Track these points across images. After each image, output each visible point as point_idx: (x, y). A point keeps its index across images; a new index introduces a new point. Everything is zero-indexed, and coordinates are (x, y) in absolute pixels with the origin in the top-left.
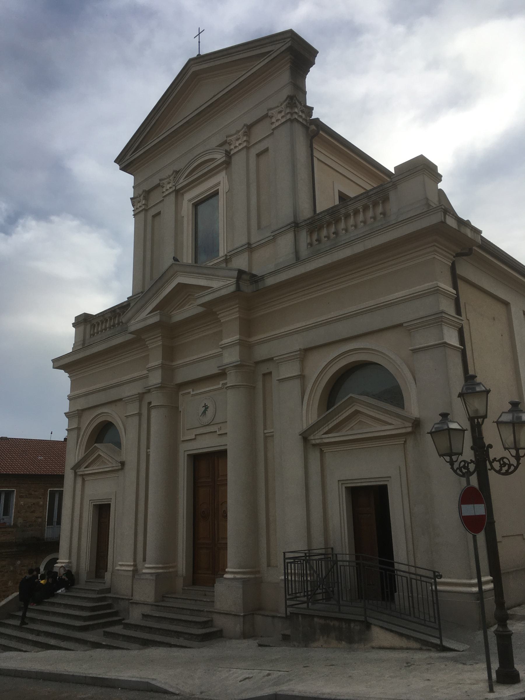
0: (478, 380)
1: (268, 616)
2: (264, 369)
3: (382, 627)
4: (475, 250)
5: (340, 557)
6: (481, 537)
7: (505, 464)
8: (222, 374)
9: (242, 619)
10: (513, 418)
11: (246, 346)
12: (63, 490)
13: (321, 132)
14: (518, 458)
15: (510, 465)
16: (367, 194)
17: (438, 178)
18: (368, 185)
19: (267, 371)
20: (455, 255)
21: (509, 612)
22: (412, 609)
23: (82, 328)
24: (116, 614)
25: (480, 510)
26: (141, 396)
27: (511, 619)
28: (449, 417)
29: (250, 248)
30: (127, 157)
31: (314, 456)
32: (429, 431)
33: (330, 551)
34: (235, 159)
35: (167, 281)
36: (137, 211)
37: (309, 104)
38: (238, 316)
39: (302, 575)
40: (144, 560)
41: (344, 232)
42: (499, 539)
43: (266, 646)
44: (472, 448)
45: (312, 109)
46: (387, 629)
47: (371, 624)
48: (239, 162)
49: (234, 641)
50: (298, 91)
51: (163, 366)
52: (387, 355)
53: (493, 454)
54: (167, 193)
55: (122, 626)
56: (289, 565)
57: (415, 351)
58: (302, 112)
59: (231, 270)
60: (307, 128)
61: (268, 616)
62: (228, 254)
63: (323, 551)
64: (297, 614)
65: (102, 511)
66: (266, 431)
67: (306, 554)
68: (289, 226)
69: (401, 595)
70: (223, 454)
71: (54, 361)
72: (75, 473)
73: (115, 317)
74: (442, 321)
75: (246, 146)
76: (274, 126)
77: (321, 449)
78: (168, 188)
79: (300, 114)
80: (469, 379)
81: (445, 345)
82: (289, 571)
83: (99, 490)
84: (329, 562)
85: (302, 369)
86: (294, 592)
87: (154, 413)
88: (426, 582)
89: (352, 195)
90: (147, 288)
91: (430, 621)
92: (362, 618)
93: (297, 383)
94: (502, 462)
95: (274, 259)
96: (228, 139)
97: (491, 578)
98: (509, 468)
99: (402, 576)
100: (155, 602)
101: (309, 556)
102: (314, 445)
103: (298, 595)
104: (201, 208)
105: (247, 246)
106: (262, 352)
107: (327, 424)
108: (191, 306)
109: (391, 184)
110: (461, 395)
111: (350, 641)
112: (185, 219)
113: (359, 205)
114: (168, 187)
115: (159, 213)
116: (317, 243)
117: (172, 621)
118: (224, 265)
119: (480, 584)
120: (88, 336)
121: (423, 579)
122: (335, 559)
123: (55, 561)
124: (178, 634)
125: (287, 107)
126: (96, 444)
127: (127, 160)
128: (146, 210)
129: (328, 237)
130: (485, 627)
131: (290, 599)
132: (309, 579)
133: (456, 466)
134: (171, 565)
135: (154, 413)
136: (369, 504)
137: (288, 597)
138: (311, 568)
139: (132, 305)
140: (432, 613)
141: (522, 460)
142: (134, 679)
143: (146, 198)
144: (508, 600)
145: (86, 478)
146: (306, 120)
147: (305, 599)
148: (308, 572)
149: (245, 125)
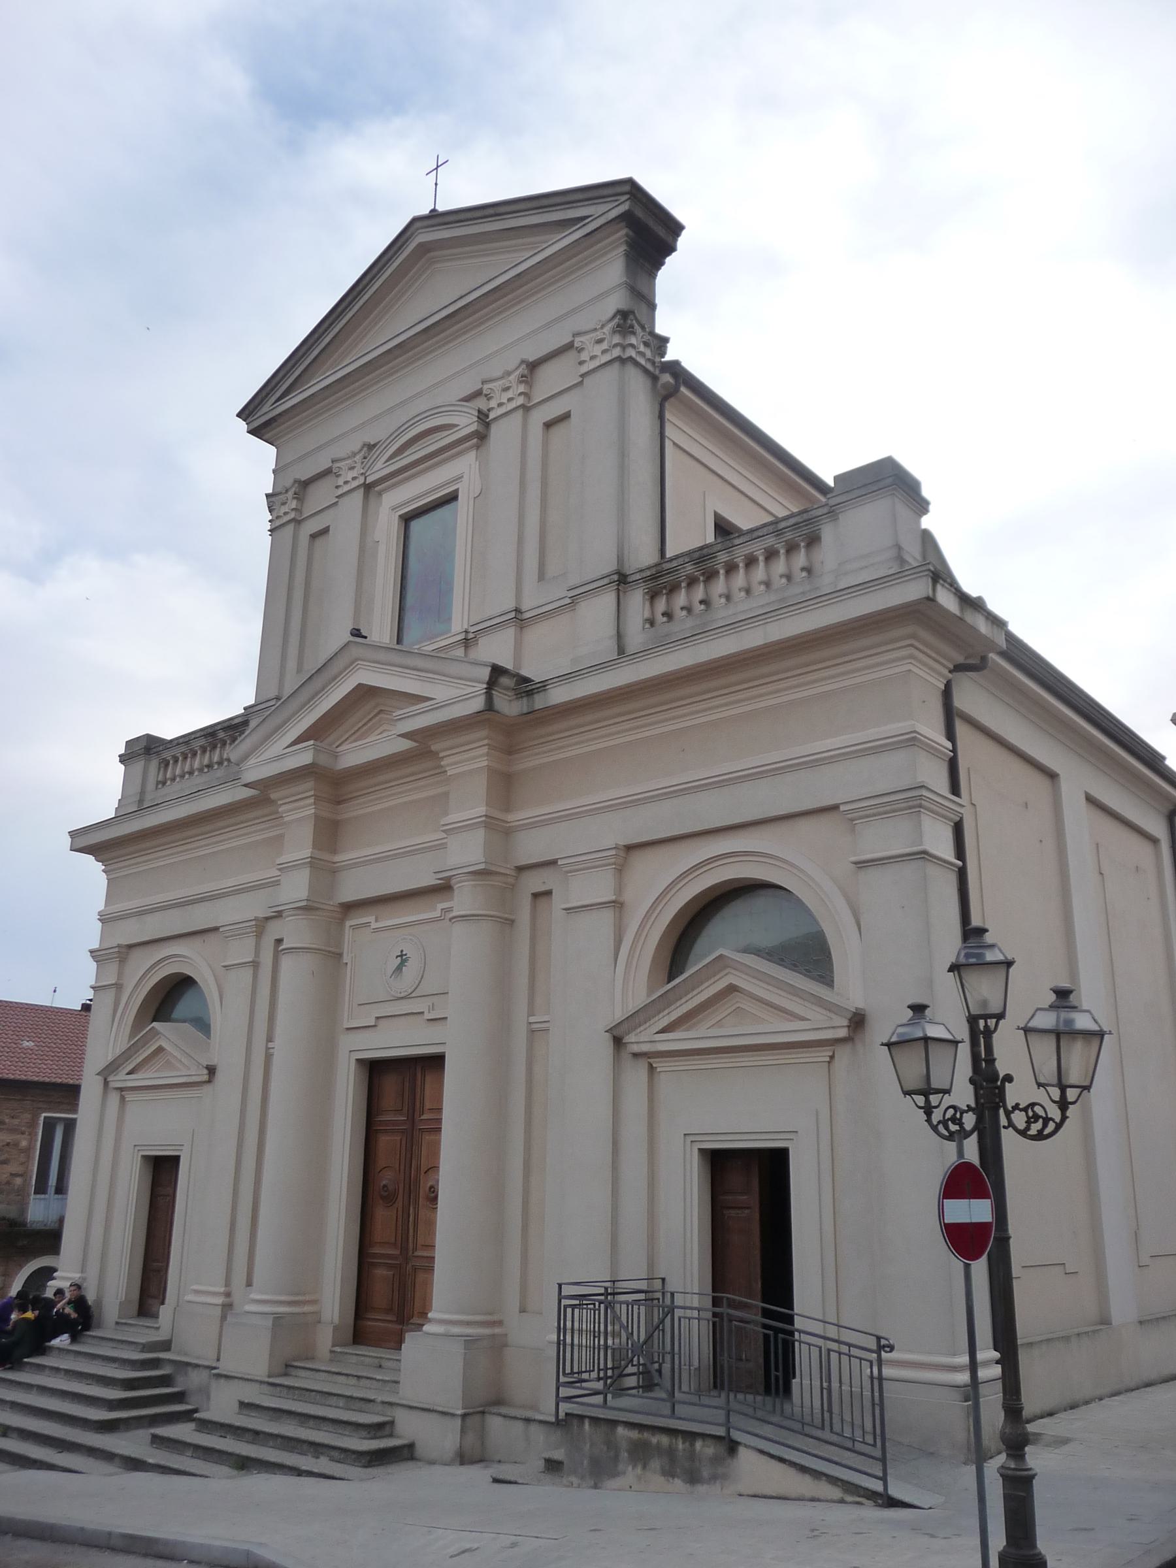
0: (989, 938)
1: (515, 1418)
2: (535, 882)
3: (762, 1452)
4: (993, 660)
5: (679, 1300)
6: (980, 1267)
7: (1036, 1117)
8: (444, 888)
9: (459, 1422)
10: (1058, 1021)
11: (498, 829)
12: (75, 1120)
13: (683, 389)
14: (1063, 1105)
15: (1046, 1120)
16: (775, 527)
17: (922, 506)
18: (781, 506)
19: (543, 888)
20: (951, 667)
21: (1031, 1428)
22: (827, 1415)
23: (139, 766)
24: (180, 1397)
25: (978, 1211)
26: (261, 925)
27: (1034, 1443)
28: (927, 1012)
29: (519, 619)
30: (265, 409)
31: (636, 1076)
32: (885, 1041)
33: (657, 1284)
34: (497, 432)
35: (335, 678)
36: (278, 523)
37: (660, 329)
38: (486, 763)
39: (595, 1335)
40: (249, 1284)
41: (723, 600)
42: (1016, 1271)
43: (510, 1482)
44: (971, 1081)
45: (665, 340)
46: (772, 1456)
47: (738, 1443)
48: (504, 434)
49: (438, 1470)
50: (635, 316)
51: (314, 863)
52: (792, 865)
53: (1013, 1095)
54: (346, 488)
55: (192, 1426)
56: (569, 1310)
57: (862, 865)
58: (646, 344)
59: (475, 663)
60: (655, 379)
61: (515, 1418)
62: (472, 629)
63: (643, 1285)
64: (581, 1418)
65: (162, 1170)
66: (532, 1019)
67: (606, 1289)
68: (606, 581)
69: (806, 1384)
70: (436, 1062)
71: (73, 834)
72: (106, 1083)
73: (214, 747)
74: (920, 806)
75: (523, 406)
76: (584, 369)
77: (650, 1065)
78: (281, 514)
79: (642, 348)
80: (972, 933)
81: (924, 855)
82: (569, 1324)
83: (157, 1125)
84: (656, 1309)
85: (620, 888)
86: (576, 1370)
87: (286, 963)
88: (861, 1359)
89: (745, 525)
90: (288, 690)
91: (863, 1442)
92: (721, 1432)
93: (607, 917)
94: (1030, 1114)
95: (570, 650)
96: (486, 387)
97: (997, 1355)
98: (1045, 1125)
99: (809, 1345)
100: (269, 1377)
101: (614, 1294)
102: (636, 1055)
103: (585, 1376)
104: (415, 525)
105: (513, 615)
106: (531, 847)
107: (666, 1012)
108: (385, 735)
109: (825, 510)
110: (954, 968)
111: (693, 1478)
112: (382, 548)
113: (757, 548)
114: (349, 477)
115: (325, 531)
116: (665, 619)
117: (304, 1418)
118: (460, 652)
119: (973, 1366)
120: (151, 785)
121: (854, 1351)
122: (668, 1301)
123: (47, 1273)
124: (317, 1448)
125: (614, 332)
126: (154, 1024)
127: (264, 415)
128: (297, 522)
129: (688, 609)
130: (980, 1457)
131: (570, 1384)
132: (610, 1342)
133: (937, 1116)
134: (307, 1298)
135: (287, 964)
136: (751, 1190)
137: (562, 1379)
138: (617, 1318)
139: (253, 724)
140: (868, 1426)
141: (1071, 1111)
142: (217, 1543)
143: (300, 497)
144: (1030, 1403)
145: (129, 1097)
146: (653, 363)
147: (600, 1385)
148: (609, 1328)
149: (295, 481)
